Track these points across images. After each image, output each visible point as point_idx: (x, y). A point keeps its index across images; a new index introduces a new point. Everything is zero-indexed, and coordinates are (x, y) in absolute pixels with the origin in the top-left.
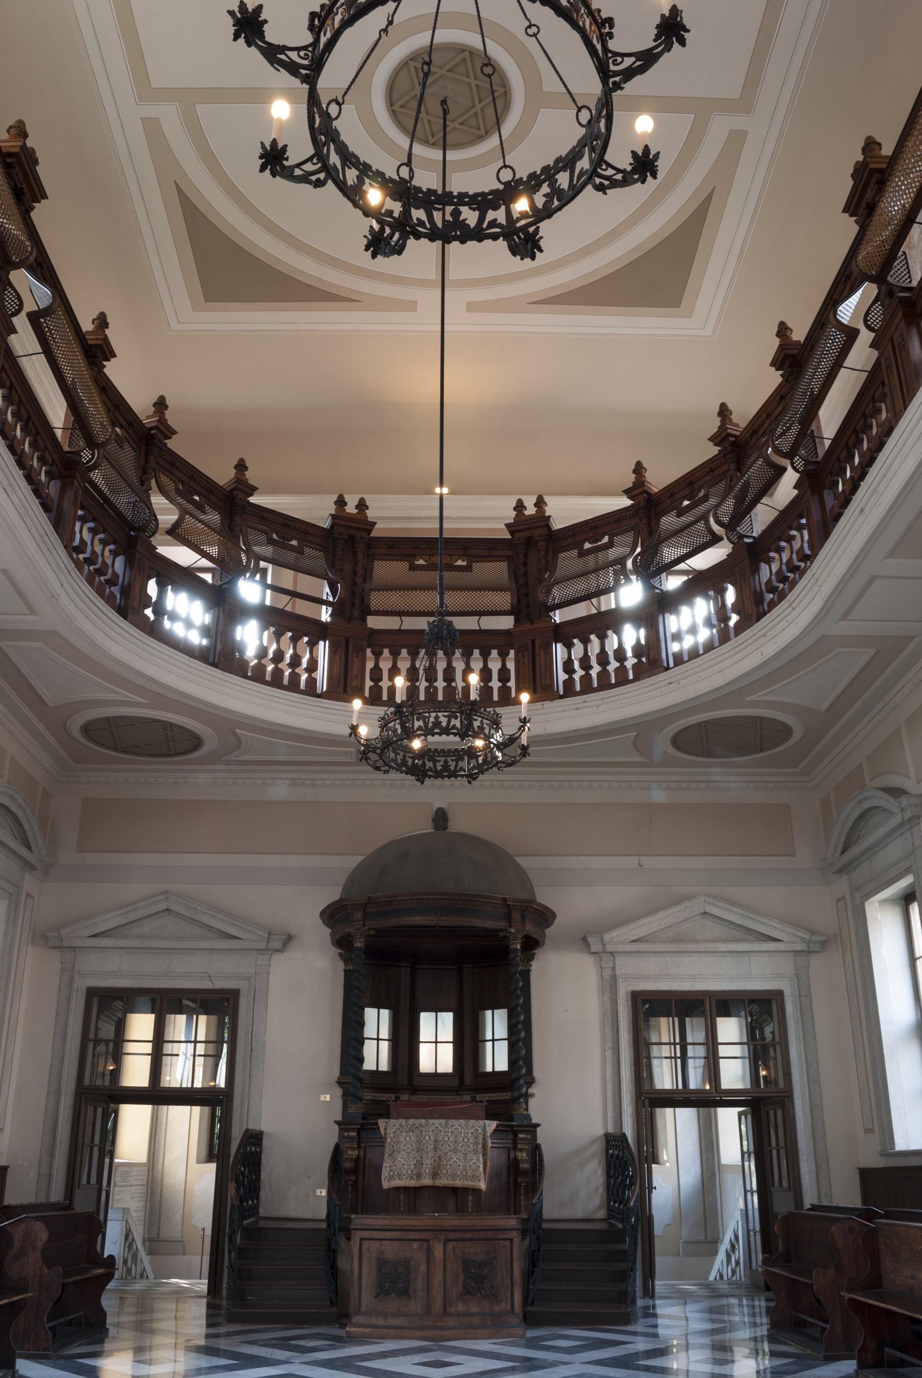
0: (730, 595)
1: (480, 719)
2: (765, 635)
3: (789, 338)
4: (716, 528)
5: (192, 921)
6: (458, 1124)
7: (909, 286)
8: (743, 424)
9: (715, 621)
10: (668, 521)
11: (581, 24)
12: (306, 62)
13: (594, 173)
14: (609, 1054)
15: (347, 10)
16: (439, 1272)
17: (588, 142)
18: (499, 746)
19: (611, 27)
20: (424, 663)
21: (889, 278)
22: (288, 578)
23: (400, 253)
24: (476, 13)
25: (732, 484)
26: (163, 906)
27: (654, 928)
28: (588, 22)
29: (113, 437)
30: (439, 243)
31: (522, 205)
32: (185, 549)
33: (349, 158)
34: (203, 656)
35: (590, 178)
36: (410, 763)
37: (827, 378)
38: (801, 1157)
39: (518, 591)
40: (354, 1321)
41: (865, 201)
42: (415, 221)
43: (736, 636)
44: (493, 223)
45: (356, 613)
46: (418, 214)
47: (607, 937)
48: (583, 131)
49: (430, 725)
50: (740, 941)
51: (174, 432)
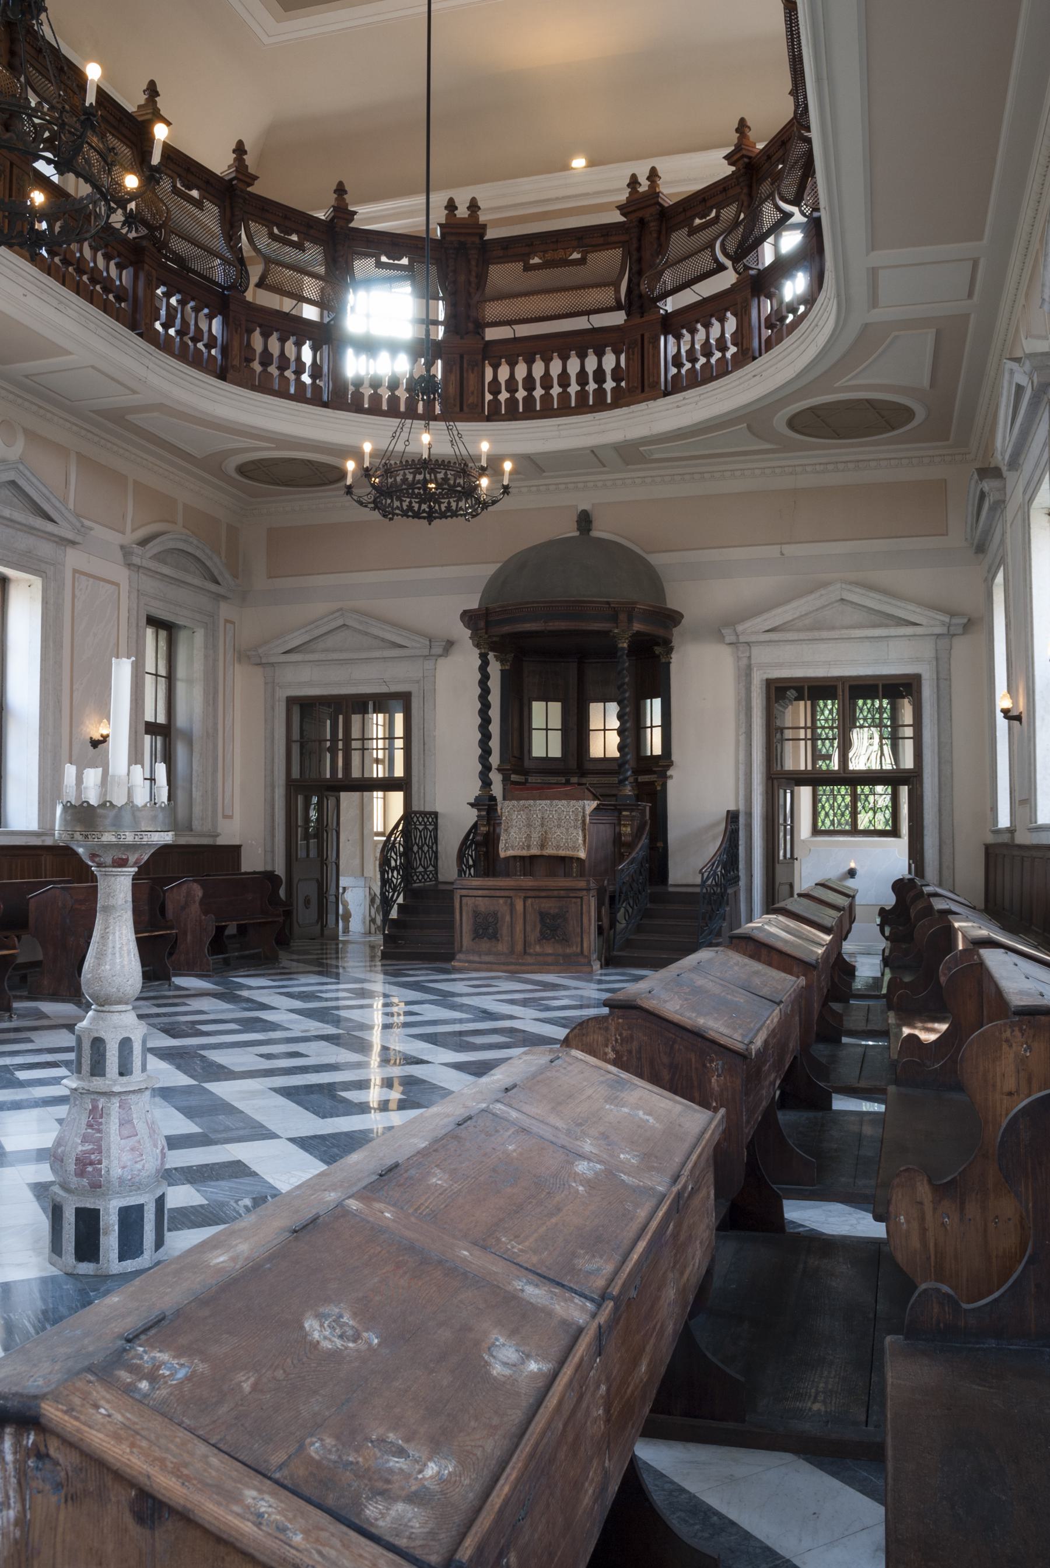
5: (366, 634)
6: (561, 804)
14: (742, 738)
16: (521, 921)
26: (340, 622)
27: (788, 617)
38: (925, 832)
40: (457, 957)
47: (740, 628)
50: (887, 626)
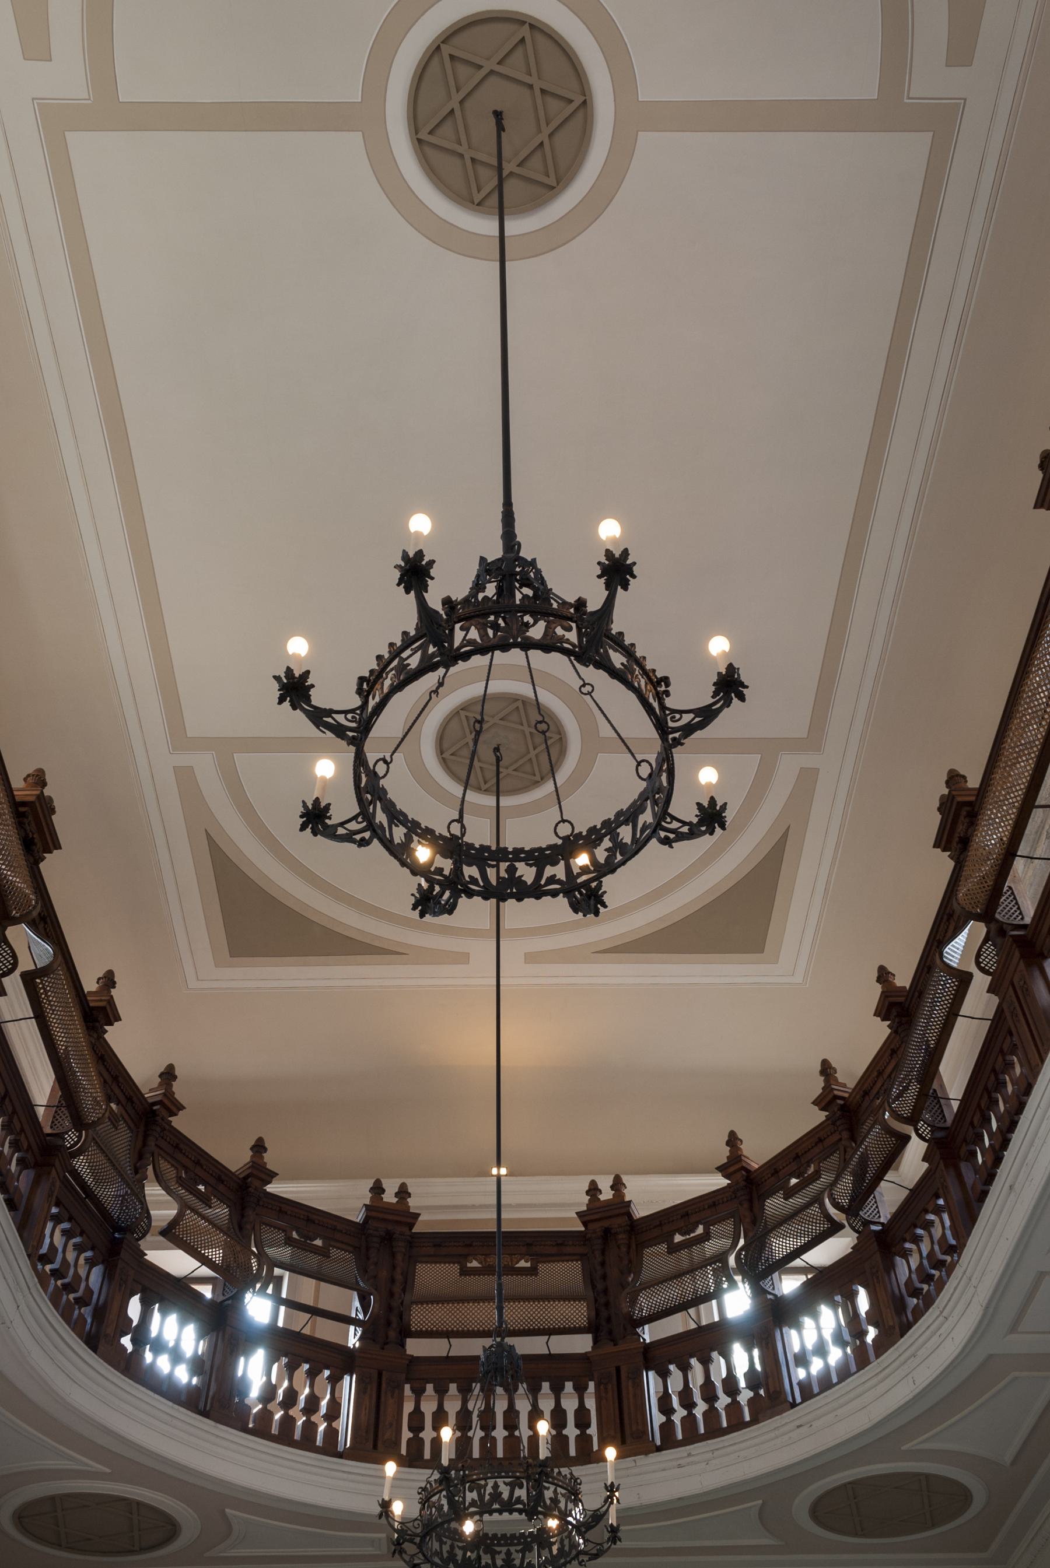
0: (863, 1302)
1: (552, 1488)
2: (914, 1355)
3: (892, 984)
4: (832, 1211)
7: (1021, 923)
8: (851, 1084)
9: (847, 1337)
10: (775, 1205)
11: (636, 684)
12: (354, 725)
13: (658, 826)
15: (397, 675)
17: (650, 795)
18: (582, 1528)
19: (667, 685)
20: (479, 1403)
21: (997, 916)
22: (308, 1290)
23: (450, 912)
24: (526, 664)
25: (848, 1157)
28: (643, 682)
29: (107, 1115)
30: (494, 901)
31: (583, 859)
32: (180, 1253)
33: (396, 816)
34: (194, 1401)
35: (654, 831)
36: (459, 1558)
37: (943, 1028)
39: (596, 1301)
41: (957, 835)
42: (467, 879)
43: (877, 1357)
44: (552, 880)
45: (392, 1334)
46: (470, 871)
48: (644, 784)
49: (487, 1497)
51: (181, 1107)
